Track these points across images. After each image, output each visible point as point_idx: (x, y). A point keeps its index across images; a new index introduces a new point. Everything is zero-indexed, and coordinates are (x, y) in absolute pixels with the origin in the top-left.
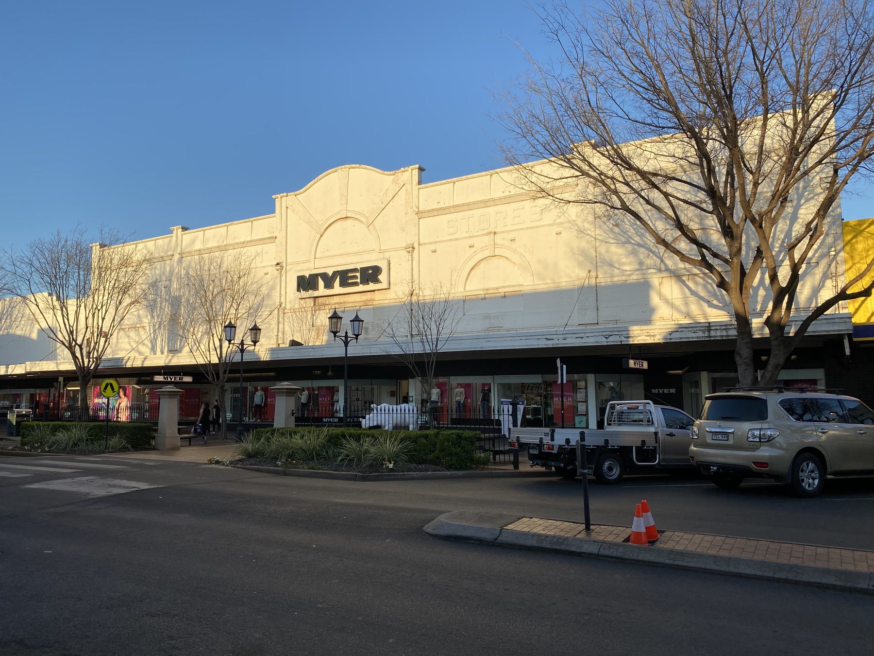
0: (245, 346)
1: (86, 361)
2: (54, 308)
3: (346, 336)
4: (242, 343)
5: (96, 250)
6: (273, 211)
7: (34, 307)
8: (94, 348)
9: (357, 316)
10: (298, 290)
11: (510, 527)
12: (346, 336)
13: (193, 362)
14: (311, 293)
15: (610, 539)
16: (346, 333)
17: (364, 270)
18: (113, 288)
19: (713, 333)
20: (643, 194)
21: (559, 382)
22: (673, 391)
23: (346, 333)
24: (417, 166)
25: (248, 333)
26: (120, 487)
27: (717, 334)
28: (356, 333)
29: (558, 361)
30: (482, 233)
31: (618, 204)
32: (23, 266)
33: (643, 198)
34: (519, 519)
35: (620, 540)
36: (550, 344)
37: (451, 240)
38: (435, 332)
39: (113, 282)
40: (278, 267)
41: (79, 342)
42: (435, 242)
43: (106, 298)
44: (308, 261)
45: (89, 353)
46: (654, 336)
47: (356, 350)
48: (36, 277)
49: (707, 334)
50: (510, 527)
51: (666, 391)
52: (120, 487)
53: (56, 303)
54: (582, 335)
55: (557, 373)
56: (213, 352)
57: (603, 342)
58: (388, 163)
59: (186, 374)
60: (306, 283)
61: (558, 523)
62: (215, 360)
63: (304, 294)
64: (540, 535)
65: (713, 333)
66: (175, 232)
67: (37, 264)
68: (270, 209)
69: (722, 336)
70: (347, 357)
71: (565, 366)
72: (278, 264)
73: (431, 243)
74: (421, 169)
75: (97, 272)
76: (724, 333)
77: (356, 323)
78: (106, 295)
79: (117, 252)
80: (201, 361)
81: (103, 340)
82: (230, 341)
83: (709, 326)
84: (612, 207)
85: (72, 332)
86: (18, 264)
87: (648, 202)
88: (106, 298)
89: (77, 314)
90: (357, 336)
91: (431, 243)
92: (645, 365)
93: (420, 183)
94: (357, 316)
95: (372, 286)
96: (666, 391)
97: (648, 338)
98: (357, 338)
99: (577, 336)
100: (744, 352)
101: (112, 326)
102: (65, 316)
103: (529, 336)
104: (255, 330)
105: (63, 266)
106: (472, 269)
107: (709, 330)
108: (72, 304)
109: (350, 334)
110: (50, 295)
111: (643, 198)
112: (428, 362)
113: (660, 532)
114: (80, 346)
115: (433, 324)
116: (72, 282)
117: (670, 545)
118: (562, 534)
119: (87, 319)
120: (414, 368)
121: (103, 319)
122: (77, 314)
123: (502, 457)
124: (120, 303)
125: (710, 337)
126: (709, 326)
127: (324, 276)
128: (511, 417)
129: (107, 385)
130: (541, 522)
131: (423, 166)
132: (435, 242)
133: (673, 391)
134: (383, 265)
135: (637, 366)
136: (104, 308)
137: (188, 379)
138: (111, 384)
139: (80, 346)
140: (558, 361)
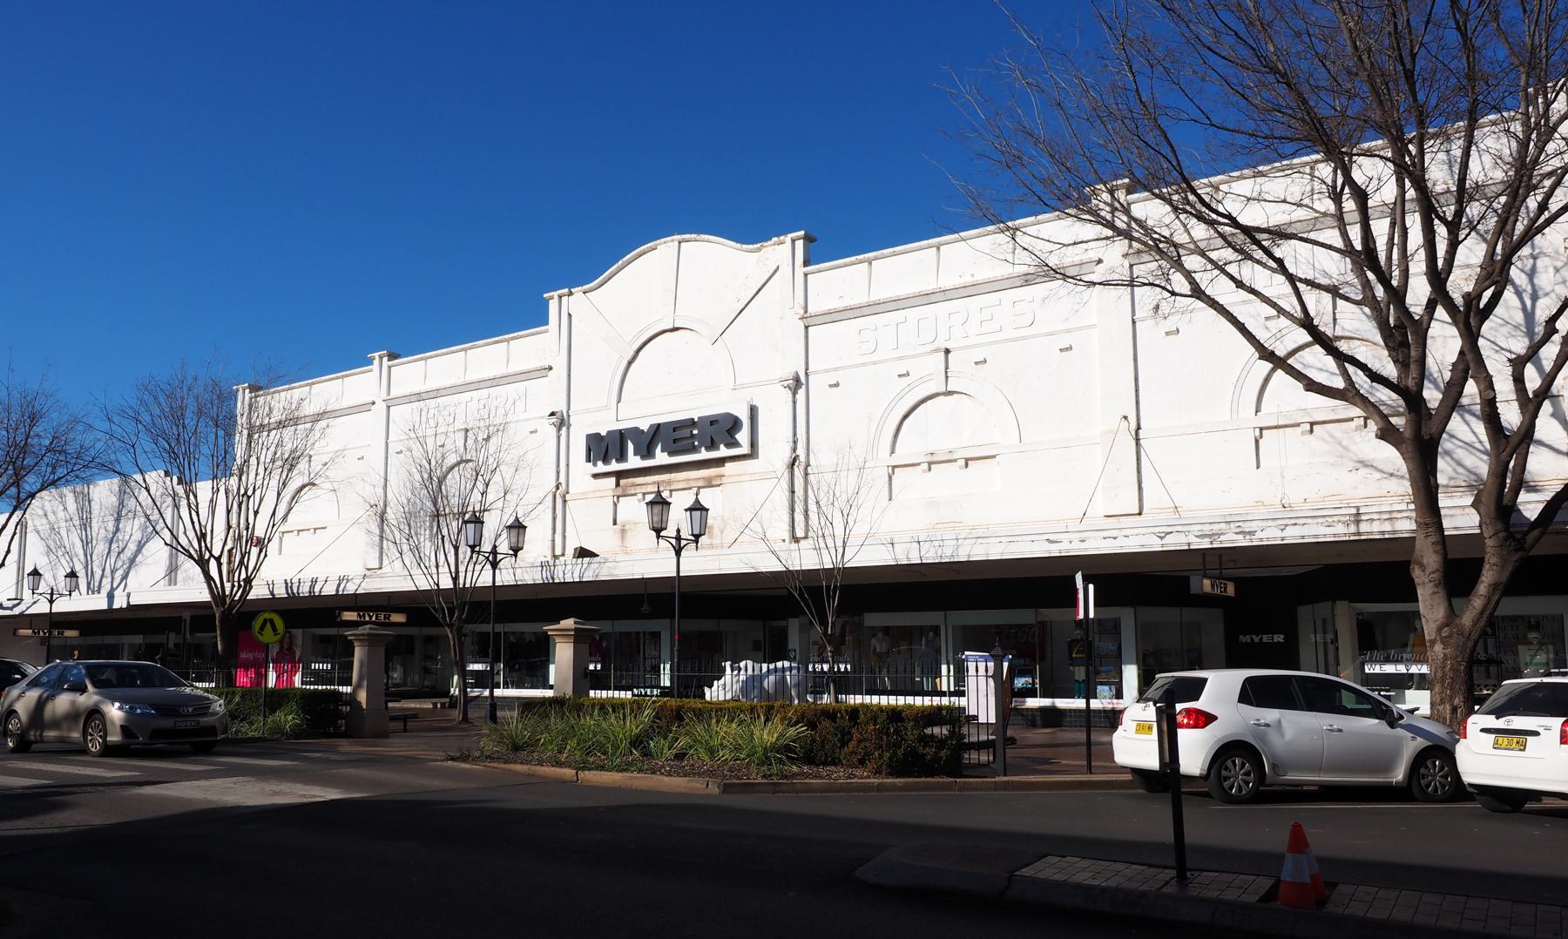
0: (499, 557)
1: (228, 586)
2: (175, 496)
3: (678, 538)
4: (494, 552)
5: (244, 396)
6: (544, 321)
7: (143, 496)
8: (241, 562)
9: (697, 501)
10: (588, 460)
11: (1027, 872)
12: (678, 538)
13: (406, 586)
14: (614, 466)
15: (1230, 895)
16: (678, 531)
17: (713, 421)
18: (273, 461)
19: (1364, 527)
20: (1229, 269)
21: (1081, 616)
22: (1279, 638)
23: (678, 531)
24: (802, 233)
25: (504, 535)
26: (292, 794)
27: (1373, 529)
28: (696, 532)
29: (1079, 578)
30: (923, 349)
31: (1186, 289)
32: (125, 423)
33: (1232, 278)
34: (1040, 858)
35: (1254, 899)
36: (1054, 551)
37: (864, 365)
38: (839, 531)
39: (272, 449)
40: (553, 419)
41: (216, 553)
42: (836, 369)
43: (260, 477)
44: (606, 407)
45: (231, 572)
46: (1252, 533)
47: (696, 564)
48: (145, 443)
49: (1353, 529)
50: (1027, 872)
51: (1265, 638)
52: (292, 794)
53: (180, 490)
54: (1113, 533)
55: (1075, 604)
56: (444, 569)
57: (1155, 545)
58: (748, 229)
59: (398, 610)
60: (604, 447)
61: (1119, 866)
62: (446, 583)
63: (601, 467)
64: (1090, 888)
65: (1364, 527)
66: (376, 362)
67: (146, 418)
68: (539, 318)
69: (1383, 533)
70: (679, 578)
71: (1091, 587)
72: (553, 414)
73: (826, 371)
74: (808, 239)
75: (245, 432)
76: (1387, 527)
77: (697, 514)
78: (261, 470)
79: (280, 400)
80: (424, 584)
81: (255, 551)
82: (472, 547)
83: (1358, 514)
84: (1173, 293)
85: (204, 535)
86: (116, 419)
87: (1240, 284)
88: (260, 477)
89: (213, 504)
90: (697, 537)
91: (826, 371)
92: (1231, 590)
93: (806, 263)
94: (697, 501)
95: (723, 451)
96: (1265, 638)
97: (1240, 537)
98: (697, 542)
99: (1106, 534)
100: (1429, 559)
101: (272, 525)
102: (194, 509)
103: (1013, 538)
104: (518, 527)
105: (190, 421)
106: (906, 416)
107: (1358, 522)
108: (204, 489)
109: (685, 534)
110: (167, 474)
111: (1232, 278)
112: (828, 587)
113: (1327, 884)
114: (218, 559)
115: (837, 515)
116: (205, 449)
117: (1356, 910)
118: (1133, 885)
119: (229, 512)
120: (801, 594)
121: (256, 513)
122: (213, 504)
123: (974, 755)
124: (284, 484)
125: (1359, 534)
126: (1358, 514)
127: (635, 433)
128: (991, 681)
129: (265, 621)
130: (1086, 863)
131: (813, 234)
132: (836, 369)
133: (1279, 638)
134: (744, 417)
135: (1217, 591)
136: (258, 493)
137: (398, 618)
138: (272, 621)
139: (218, 559)
140: (1079, 578)
